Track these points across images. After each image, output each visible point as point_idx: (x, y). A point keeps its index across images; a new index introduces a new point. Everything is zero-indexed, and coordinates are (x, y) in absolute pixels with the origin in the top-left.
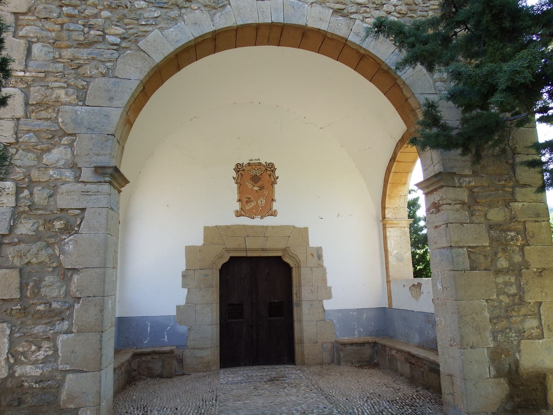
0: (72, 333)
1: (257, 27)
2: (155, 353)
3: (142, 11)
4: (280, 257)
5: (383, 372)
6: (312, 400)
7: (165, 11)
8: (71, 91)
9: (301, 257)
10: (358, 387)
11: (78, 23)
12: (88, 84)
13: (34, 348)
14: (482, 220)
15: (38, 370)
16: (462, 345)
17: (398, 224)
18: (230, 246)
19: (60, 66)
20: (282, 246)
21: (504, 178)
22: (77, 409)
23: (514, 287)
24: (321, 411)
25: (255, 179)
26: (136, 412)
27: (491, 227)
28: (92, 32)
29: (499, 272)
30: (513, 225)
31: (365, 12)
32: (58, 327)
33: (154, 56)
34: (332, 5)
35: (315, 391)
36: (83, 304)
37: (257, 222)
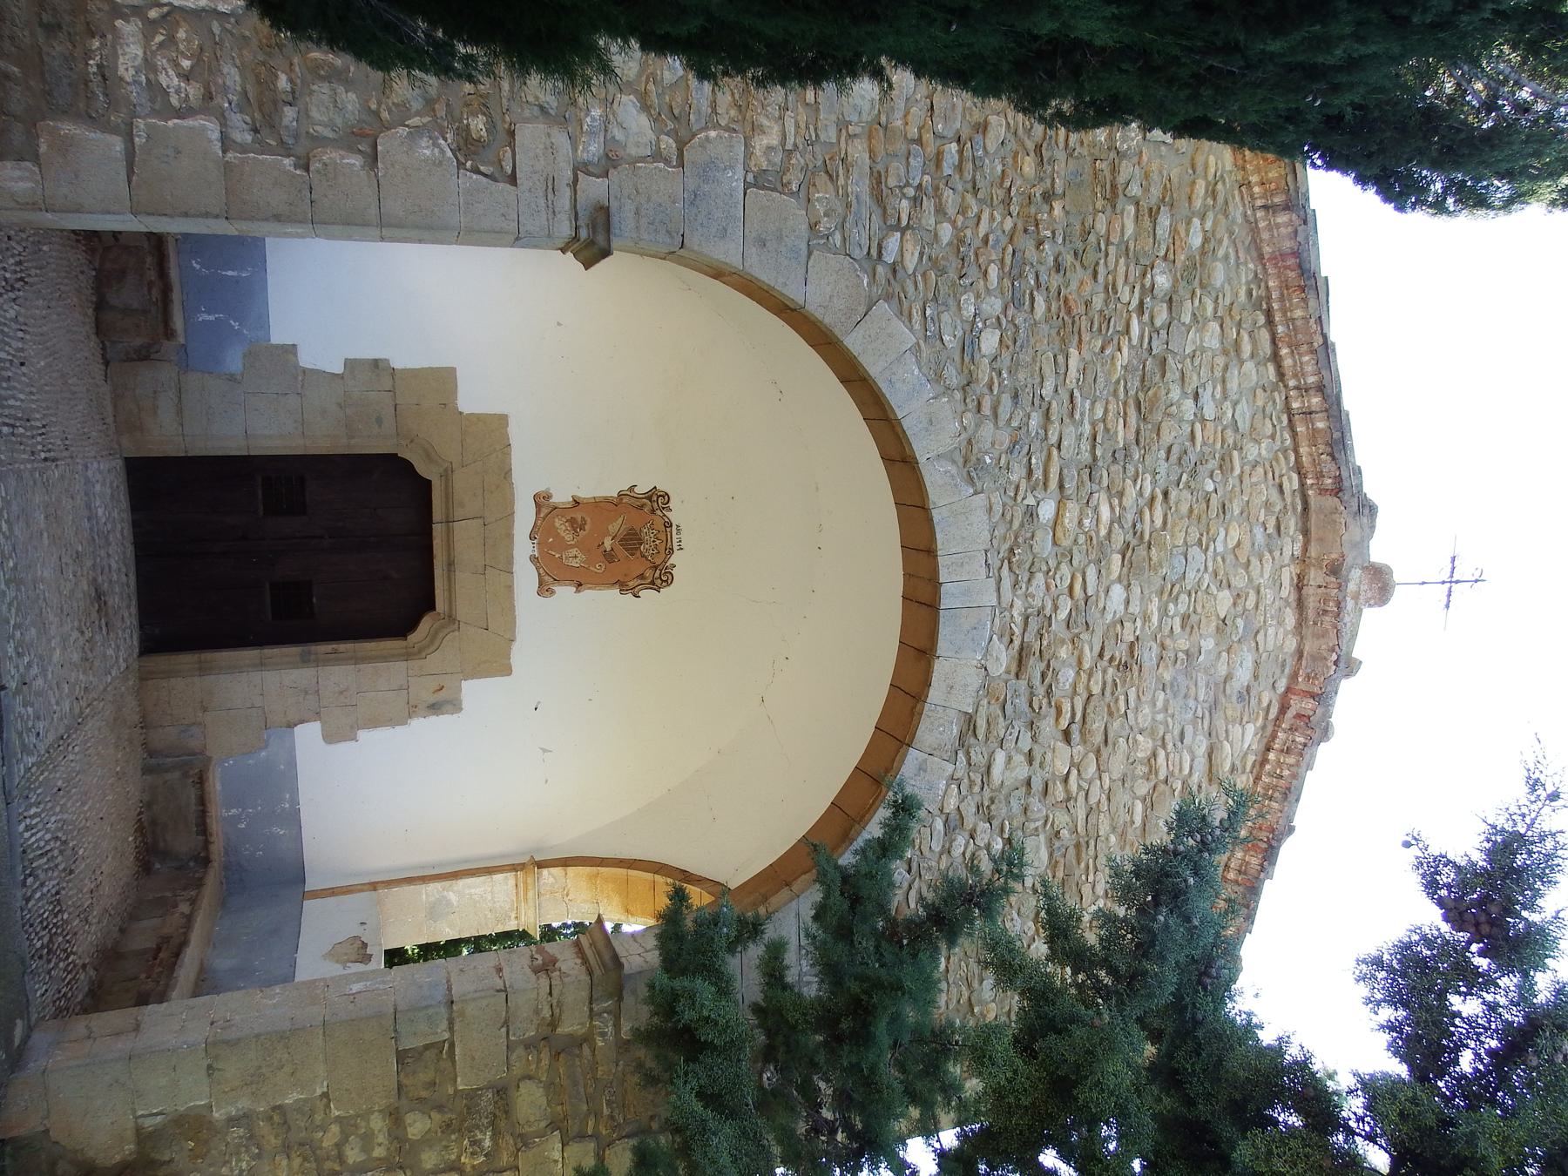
0: (224, 152)
1: (930, 552)
2: (166, 290)
3: (954, 309)
4: (432, 607)
5: (128, 884)
6: (53, 701)
7: (957, 358)
8: (778, 158)
9: (433, 661)
10: (80, 819)
11: (924, 173)
12: (792, 194)
13: (186, 64)
14: (518, 1070)
15: (131, 71)
16: (214, 1047)
17: (526, 900)
18: (460, 481)
19: (830, 135)
20: (462, 612)
21: (616, 1113)
22: (36, 158)
23: (362, 1158)
24: (30, 724)
25: (631, 541)
26: (11, 261)
27: (502, 1092)
28: (905, 203)
29: (395, 1117)
30: (508, 1142)
31: (972, 783)
32: (236, 119)
33: (859, 333)
34: (983, 712)
35: (77, 711)
36: (294, 176)
37: (523, 548)
